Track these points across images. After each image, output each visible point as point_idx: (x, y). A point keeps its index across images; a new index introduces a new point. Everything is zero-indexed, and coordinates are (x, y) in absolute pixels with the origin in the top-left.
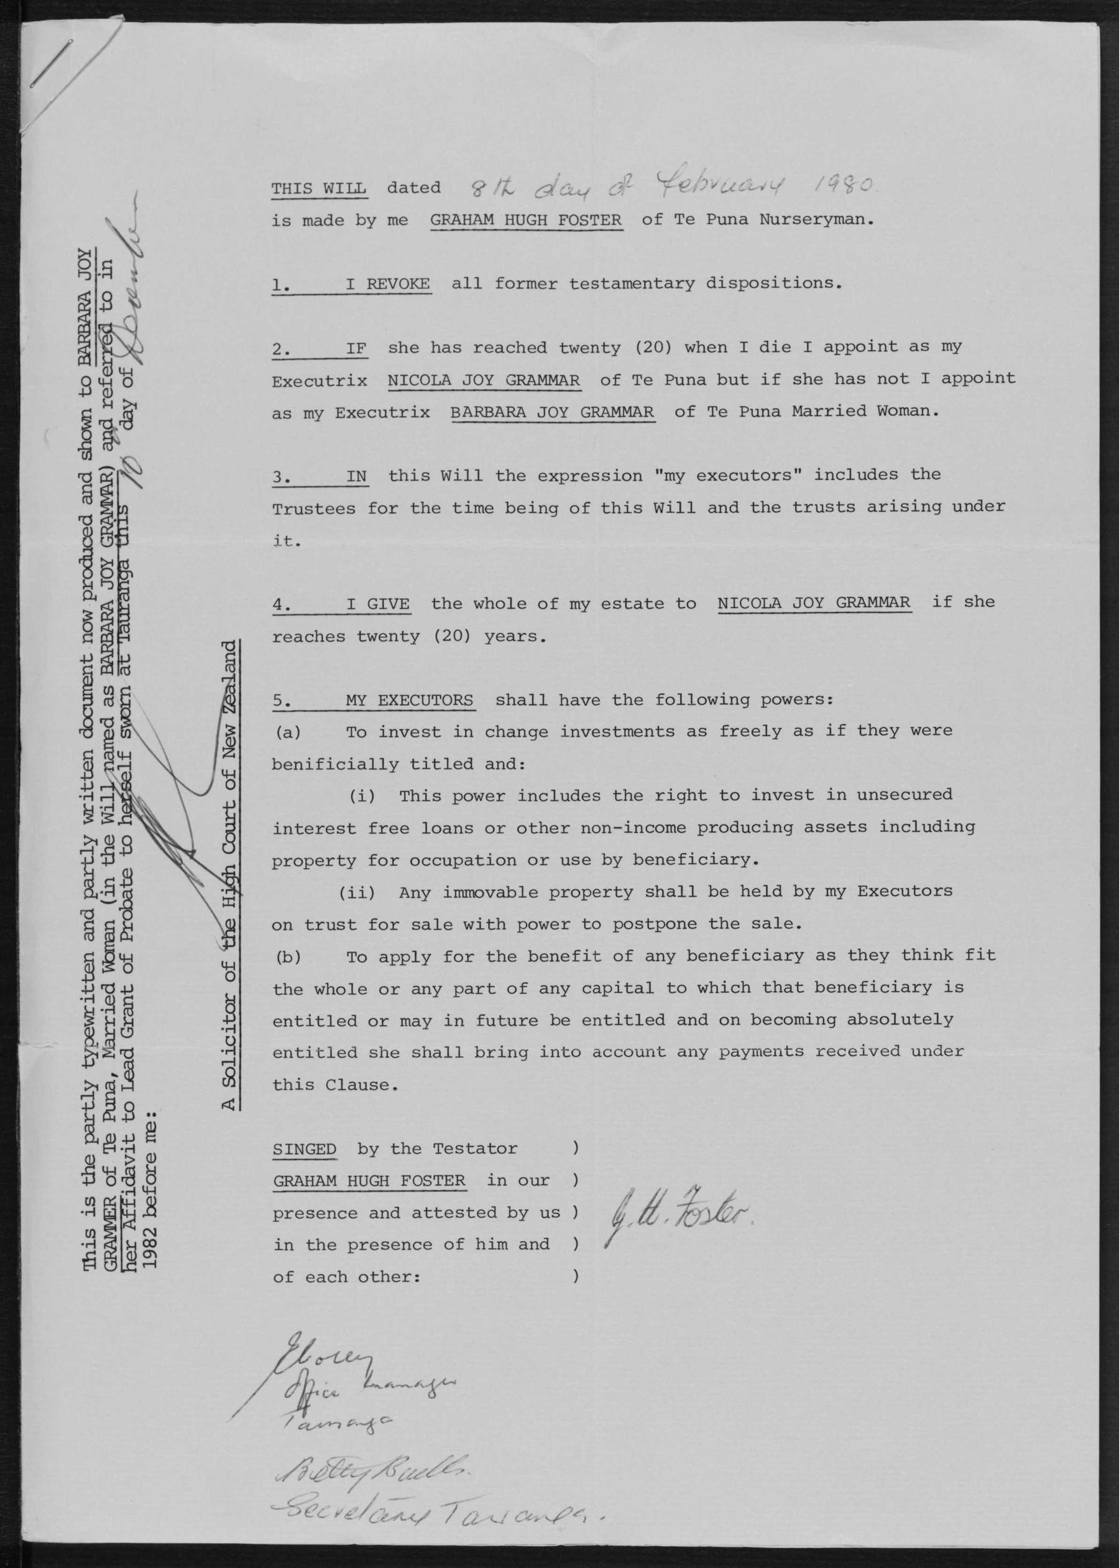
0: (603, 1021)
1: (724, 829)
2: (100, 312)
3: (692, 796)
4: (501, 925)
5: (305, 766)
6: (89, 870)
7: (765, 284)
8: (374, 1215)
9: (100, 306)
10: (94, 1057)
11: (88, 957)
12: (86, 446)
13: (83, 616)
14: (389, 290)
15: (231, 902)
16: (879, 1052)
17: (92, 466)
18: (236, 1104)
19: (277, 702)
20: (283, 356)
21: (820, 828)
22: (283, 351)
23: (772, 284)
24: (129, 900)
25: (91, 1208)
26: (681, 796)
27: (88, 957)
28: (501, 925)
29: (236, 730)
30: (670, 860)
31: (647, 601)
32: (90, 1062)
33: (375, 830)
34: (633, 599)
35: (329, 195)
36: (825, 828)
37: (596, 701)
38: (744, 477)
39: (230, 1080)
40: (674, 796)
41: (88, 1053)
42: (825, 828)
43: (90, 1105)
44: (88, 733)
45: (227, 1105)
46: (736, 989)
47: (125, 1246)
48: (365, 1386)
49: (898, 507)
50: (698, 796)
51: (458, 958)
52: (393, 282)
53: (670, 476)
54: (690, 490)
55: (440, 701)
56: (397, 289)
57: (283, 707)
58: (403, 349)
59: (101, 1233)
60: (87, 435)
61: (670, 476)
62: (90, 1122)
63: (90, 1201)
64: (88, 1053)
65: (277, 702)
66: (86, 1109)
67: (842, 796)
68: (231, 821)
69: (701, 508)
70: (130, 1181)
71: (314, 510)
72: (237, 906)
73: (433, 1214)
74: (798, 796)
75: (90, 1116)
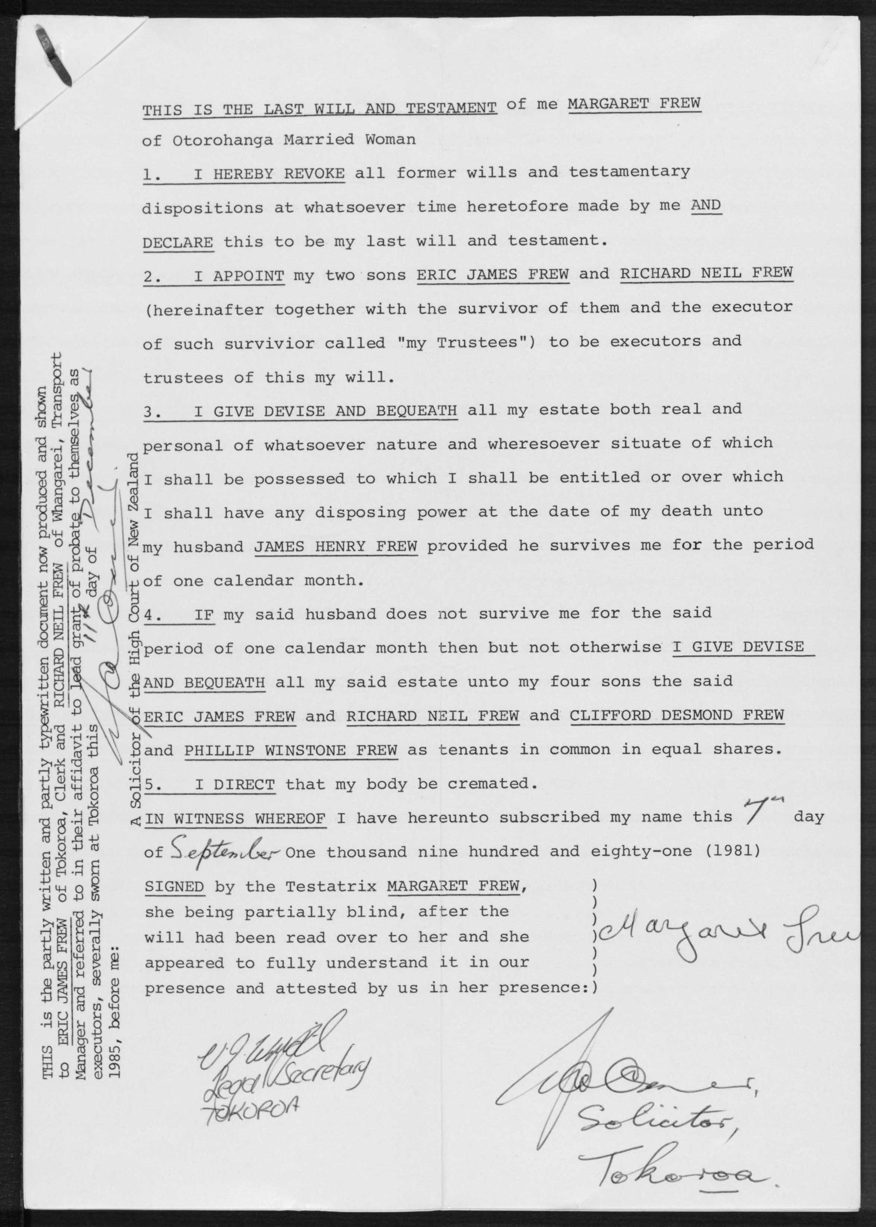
3: (626, 852)
4: (646, 410)
6: (47, 947)
8: (310, 581)
10: (49, 740)
11: (46, 855)
12: (42, 415)
13: (40, 551)
14: (306, 179)
16: (701, 477)
17: (51, 916)
20: (154, 283)
21: (412, 615)
22: (153, 278)
24: (77, 538)
25: (48, 1021)
26: (616, 852)
27: (44, 661)
28: (423, 649)
31: (583, 407)
32: (45, 744)
34: (569, 405)
38: (757, 308)
40: (609, 852)
41: (44, 737)
43: (46, 778)
44: (44, 644)
46: (422, 479)
47: (75, 1024)
48: (297, 1097)
50: (632, 852)
52: (309, 171)
53: (411, 344)
55: (313, 751)
56: (313, 178)
59: (55, 983)
60: (42, 407)
61: (411, 344)
62: (48, 952)
63: (48, 1015)
64: (44, 737)
66: (44, 941)
67: (79, 864)
70: (78, 763)
73: (296, 989)
75: (46, 787)
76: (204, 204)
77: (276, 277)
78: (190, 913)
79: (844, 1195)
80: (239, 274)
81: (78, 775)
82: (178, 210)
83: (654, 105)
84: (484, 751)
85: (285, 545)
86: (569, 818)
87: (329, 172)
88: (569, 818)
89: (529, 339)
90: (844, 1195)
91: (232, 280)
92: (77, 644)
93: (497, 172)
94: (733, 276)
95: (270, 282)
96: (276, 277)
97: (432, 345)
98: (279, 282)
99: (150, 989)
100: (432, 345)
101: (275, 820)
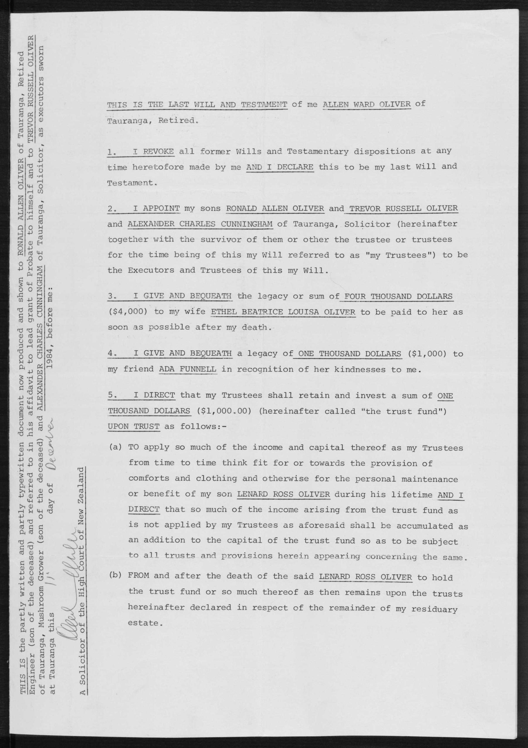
0: (30, 302)
1: (21, 357)
2: (27, 235)
5: (268, 370)
7: (382, 152)
9: (27, 232)
15: (82, 594)
18: (86, 693)
19: (110, 396)
22: (113, 209)
23: (386, 152)
29: (84, 512)
30: (161, 494)
33: (132, 463)
35: (197, 108)
36: (371, 370)
37: (192, 167)
38: (41, 99)
39: (82, 682)
42: (371, 370)
45: (82, 693)
49: (396, 464)
51: (281, 464)
53: (373, 256)
54: (433, 158)
57: (113, 398)
58: (21, 295)
61: (373, 256)
65: (110, 396)
67: (245, 608)
68: (82, 555)
69: (439, 166)
71: (325, 541)
72: (85, 596)
73: (22, 576)
74: (379, 396)
76: (385, 149)
77: (175, 209)
78: (50, 336)
79: (509, 731)
80: (156, 207)
81: (31, 400)
82: (372, 152)
83: (82, 506)
84: (30, 305)
85: (227, 311)
86: (174, 327)
87: (165, 151)
88: (174, 327)
89: (432, 253)
90: (509, 731)
91: (153, 211)
92: (30, 320)
93: (252, 151)
94: (417, 211)
95: (172, 212)
96: (175, 209)
97: (383, 257)
98: (177, 212)
99: (21, 367)
100: (383, 257)
101: (227, 313)
